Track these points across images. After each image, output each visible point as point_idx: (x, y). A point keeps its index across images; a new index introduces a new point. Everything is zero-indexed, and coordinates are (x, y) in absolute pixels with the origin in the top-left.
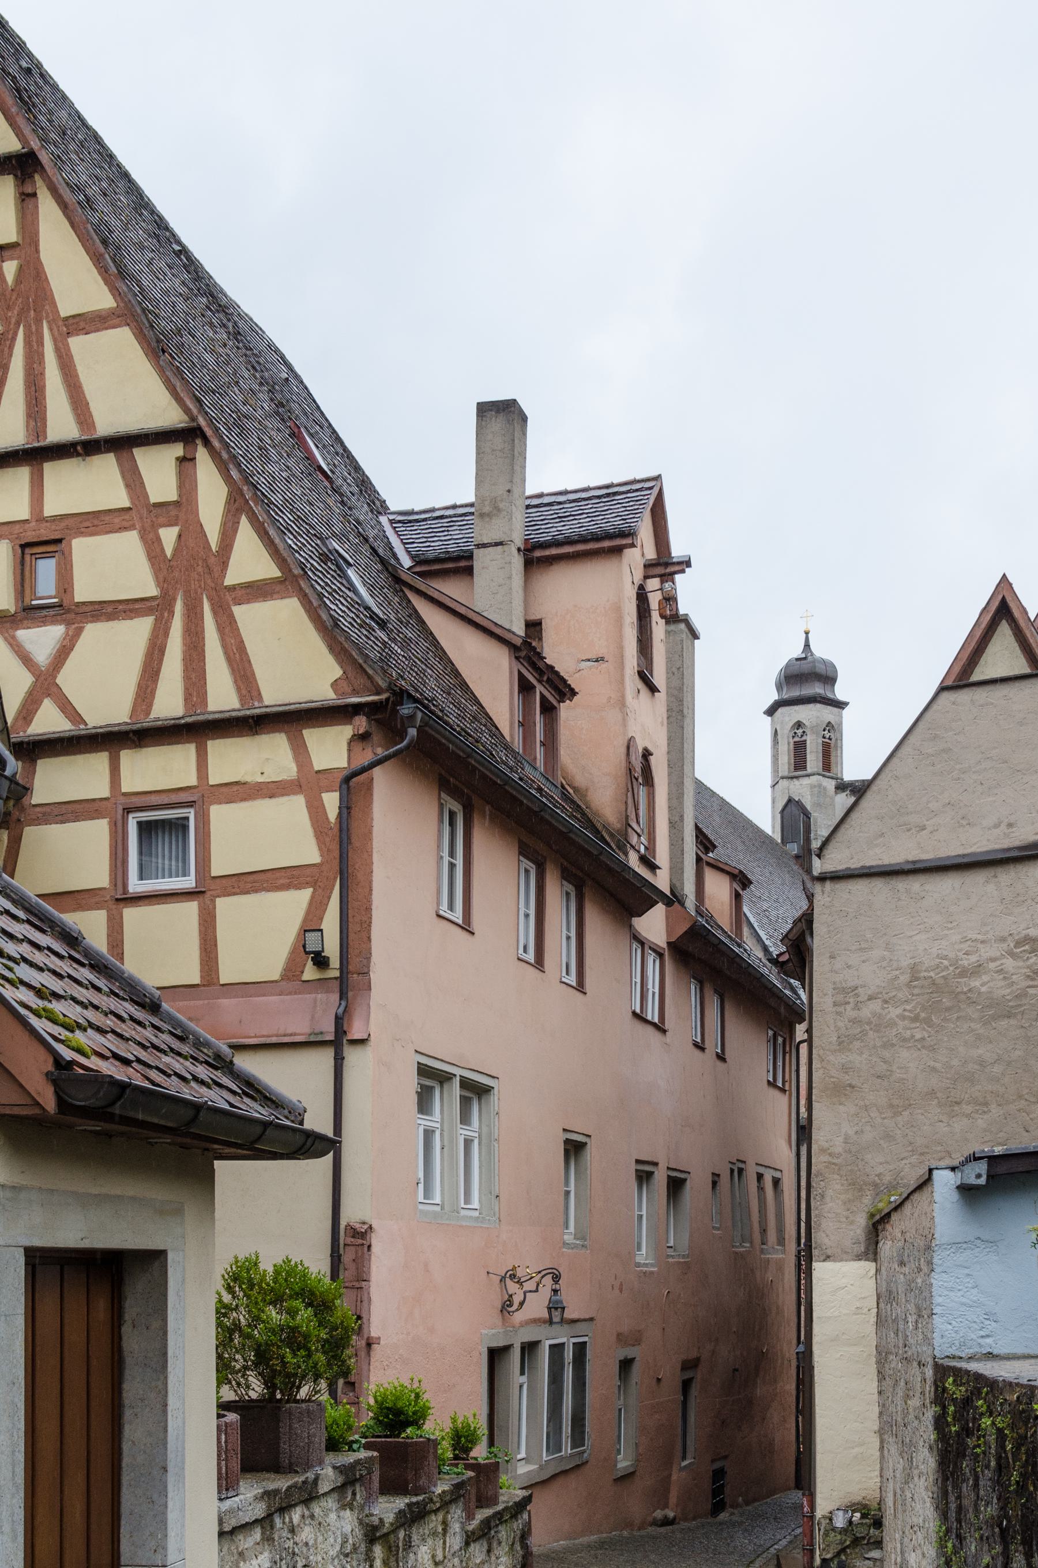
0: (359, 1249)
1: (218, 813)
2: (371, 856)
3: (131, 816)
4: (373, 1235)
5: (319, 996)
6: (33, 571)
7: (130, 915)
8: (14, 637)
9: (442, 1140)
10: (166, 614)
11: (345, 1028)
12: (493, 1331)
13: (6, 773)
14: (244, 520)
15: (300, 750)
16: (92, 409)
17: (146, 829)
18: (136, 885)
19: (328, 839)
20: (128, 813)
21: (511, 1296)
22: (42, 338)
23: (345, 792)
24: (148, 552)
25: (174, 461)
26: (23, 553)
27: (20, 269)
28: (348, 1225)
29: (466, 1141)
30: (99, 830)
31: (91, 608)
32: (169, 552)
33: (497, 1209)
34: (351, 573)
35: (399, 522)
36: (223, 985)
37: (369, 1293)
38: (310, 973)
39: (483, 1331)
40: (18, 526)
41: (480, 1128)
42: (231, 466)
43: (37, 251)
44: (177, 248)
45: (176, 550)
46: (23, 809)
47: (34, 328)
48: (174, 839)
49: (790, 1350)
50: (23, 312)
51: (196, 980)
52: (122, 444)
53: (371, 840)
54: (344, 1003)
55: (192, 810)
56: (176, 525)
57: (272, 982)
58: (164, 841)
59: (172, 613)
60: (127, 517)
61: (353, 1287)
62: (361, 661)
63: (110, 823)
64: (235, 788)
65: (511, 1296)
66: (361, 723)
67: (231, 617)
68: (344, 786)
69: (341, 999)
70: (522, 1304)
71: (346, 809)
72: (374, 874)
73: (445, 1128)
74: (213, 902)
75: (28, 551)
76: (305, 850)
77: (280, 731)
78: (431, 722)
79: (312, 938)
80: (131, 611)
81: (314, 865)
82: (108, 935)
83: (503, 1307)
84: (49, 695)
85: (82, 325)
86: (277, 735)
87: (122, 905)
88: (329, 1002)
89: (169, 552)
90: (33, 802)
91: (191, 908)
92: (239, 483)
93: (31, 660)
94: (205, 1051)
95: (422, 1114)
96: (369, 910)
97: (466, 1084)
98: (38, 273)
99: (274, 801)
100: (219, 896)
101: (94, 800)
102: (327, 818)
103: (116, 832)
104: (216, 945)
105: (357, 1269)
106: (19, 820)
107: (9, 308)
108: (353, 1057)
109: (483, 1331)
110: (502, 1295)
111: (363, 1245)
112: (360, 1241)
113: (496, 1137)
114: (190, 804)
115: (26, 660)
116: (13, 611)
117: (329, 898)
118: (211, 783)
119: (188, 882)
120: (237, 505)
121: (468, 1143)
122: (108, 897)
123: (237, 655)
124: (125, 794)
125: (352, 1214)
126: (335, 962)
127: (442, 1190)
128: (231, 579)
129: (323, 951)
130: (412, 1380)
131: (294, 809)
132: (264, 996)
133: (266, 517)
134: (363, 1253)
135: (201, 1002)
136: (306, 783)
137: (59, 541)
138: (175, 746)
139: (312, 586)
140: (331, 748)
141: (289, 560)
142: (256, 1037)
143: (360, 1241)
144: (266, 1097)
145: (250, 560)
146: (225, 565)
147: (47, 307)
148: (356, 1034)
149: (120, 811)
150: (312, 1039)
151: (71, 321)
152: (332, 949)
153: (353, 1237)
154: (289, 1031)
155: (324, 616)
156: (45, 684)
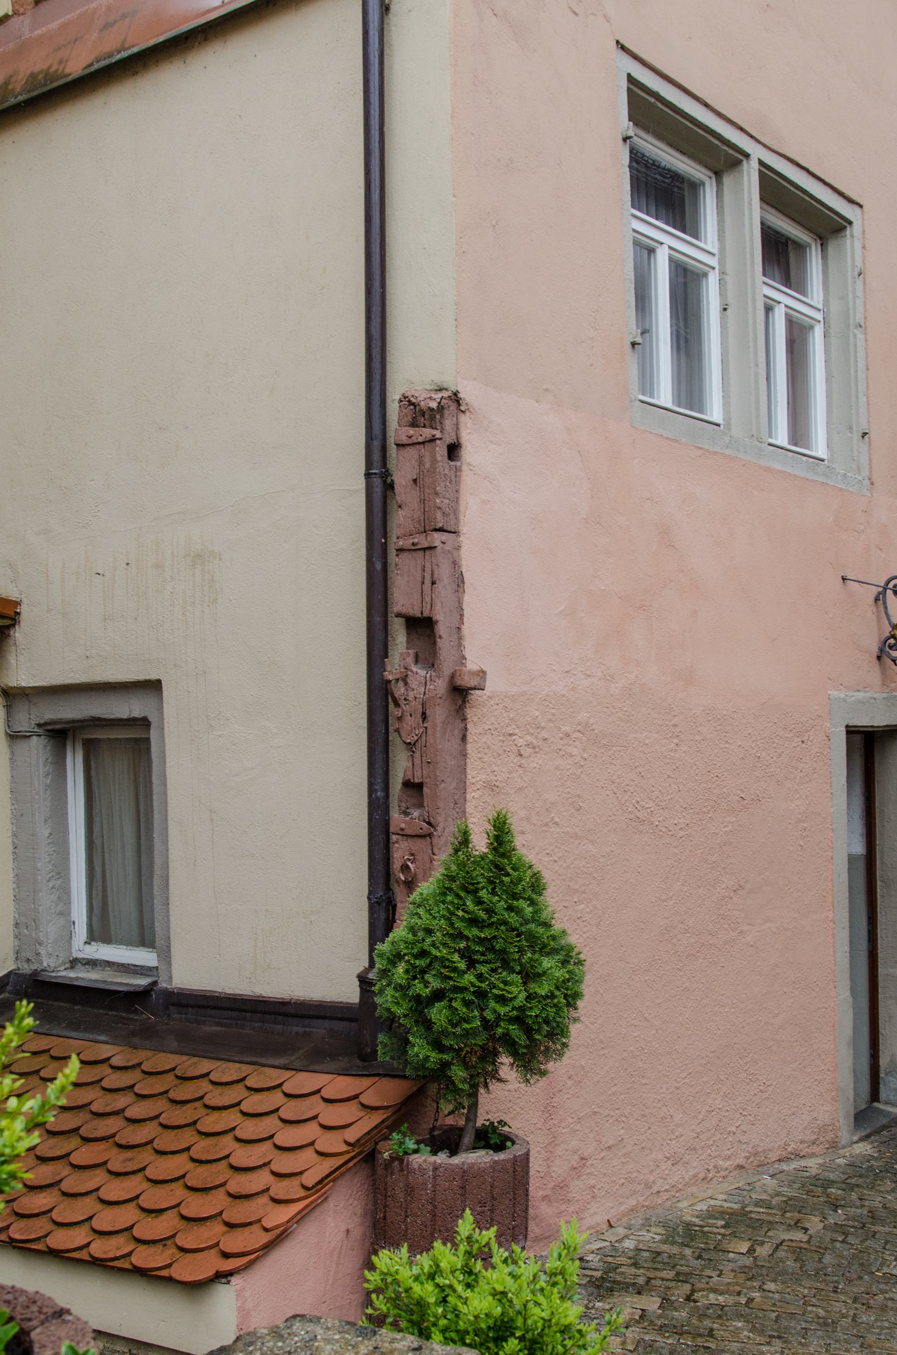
0: (425, 451)
12: (860, 695)
33: (864, 459)
37: (455, 564)
39: (834, 693)
41: (826, 302)
49: (262, 1060)
61: (414, 549)
73: (729, 268)
83: (881, 650)
95: (796, 445)
97: (776, 191)
105: (423, 501)
109: (834, 693)
112: (427, 433)
113: (859, 318)
121: (797, 334)
125: (414, 371)
127: (726, 397)
134: (434, 461)
143: (427, 433)
153: (414, 424)
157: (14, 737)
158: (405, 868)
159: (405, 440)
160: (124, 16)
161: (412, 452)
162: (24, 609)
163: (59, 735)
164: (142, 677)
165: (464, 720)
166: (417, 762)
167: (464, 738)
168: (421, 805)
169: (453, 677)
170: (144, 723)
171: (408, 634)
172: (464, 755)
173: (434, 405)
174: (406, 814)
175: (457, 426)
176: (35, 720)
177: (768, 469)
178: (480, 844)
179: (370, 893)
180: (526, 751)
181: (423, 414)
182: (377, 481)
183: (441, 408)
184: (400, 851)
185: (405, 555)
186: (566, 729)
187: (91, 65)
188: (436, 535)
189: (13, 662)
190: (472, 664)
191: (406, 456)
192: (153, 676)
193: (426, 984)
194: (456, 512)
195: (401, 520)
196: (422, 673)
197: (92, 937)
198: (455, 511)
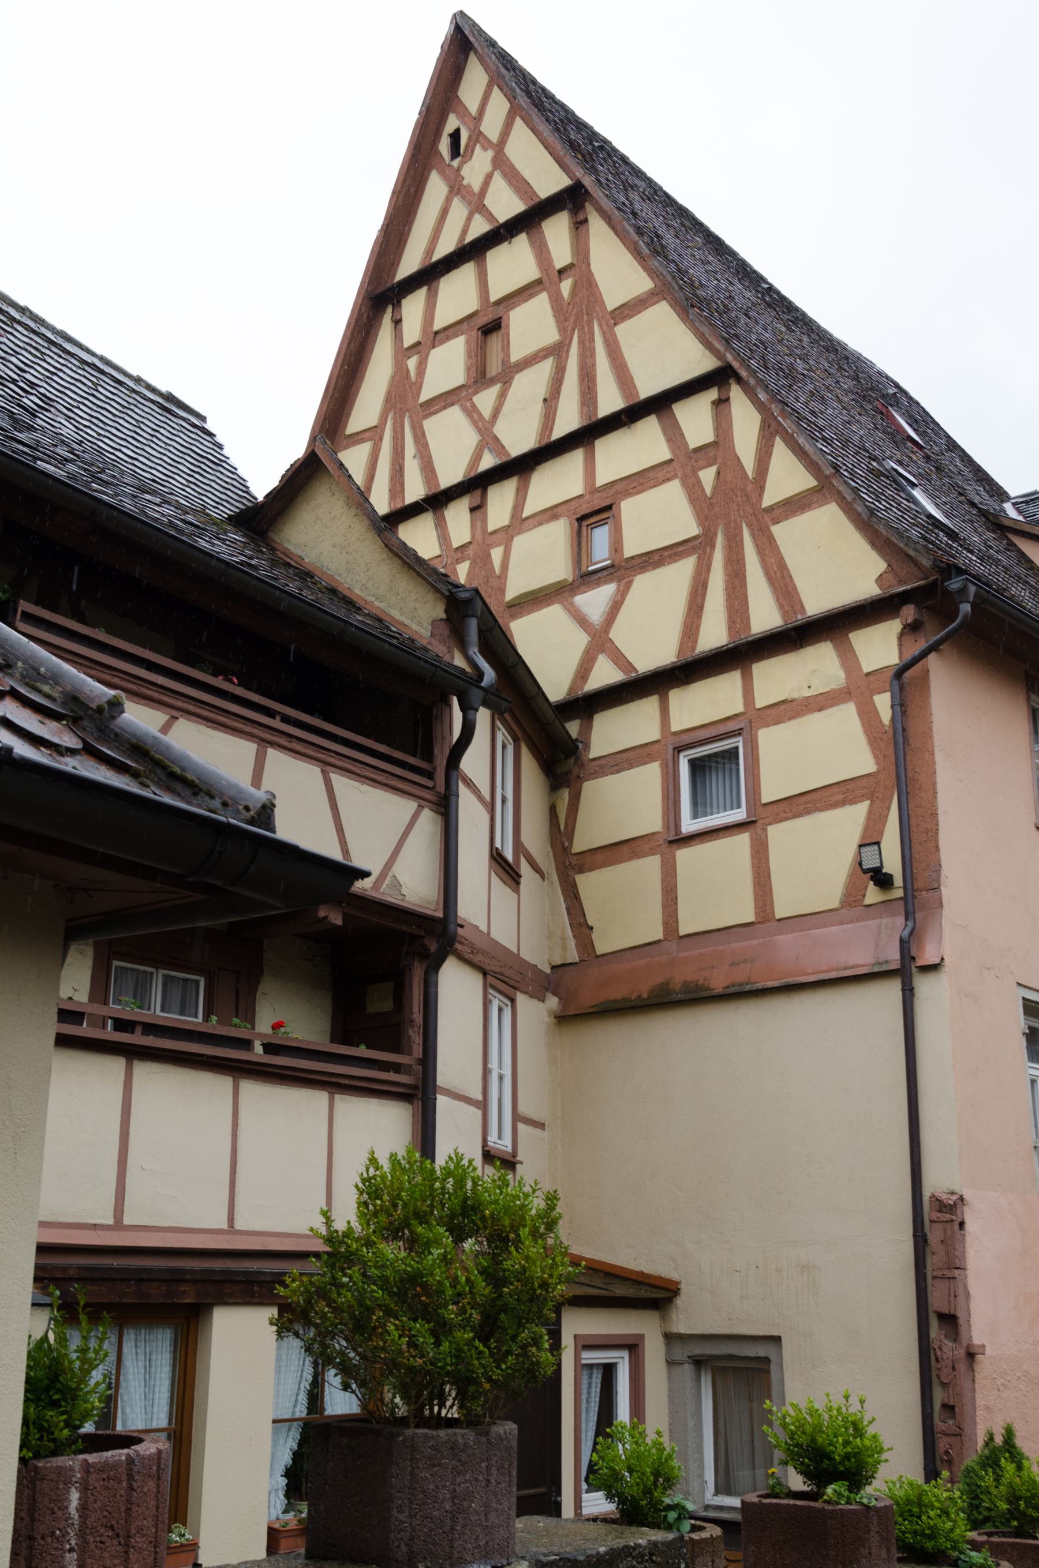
0: (948, 1226)
1: (766, 737)
2: (933, 754)
3: (682, 755)
4: (965, 1208)
5: (884, 921)
6: (589, 541)
7: (684, 856)
8: (572, 604)
10: (708, 550)
11: (913, 953)
13: (482, 684)
14: (778, 441)
15: (848, 657)
16: (637, 382)
17: (698, 767)
18: (689, 825)
19: (883, 745)
20: (679, 752)
22: (593, 335)
23: (897, 689)
24: (689, 496)
25: (709, 406)
26: (580, 526)
27: (575, 286)
28: (933, 1196)
30: (651, 774)
31: (639, 560)
32: (708, 490)
34: (917, 493)
35: (1022, 502)
36: (779, 920)
37: (965, 1286)
38: (873, 895)
40: (574, 503)
42: (759, 390)
43: (589, 265)
44: (766, 286)
45: (715, 488)
46: (582, 766)
47: (586, 329)
48: (727, 777)
50: (578, 318)
51: (751, 918)
52: (661, 404)
53: (931, 737)
54: (910, 924)
55: (740, 739)
56: (714, 464)
57: (831, 910)
58: (724, 778)
59: (713, 547)
60: (671, 468)
61: (943, 1277)
62: (901, 545)
63: (661, 765)
64: (783, 707)
66: (909, 612)
67: (771, 539)
68: (896, 682)
69: (907, 919)
71: (901, 706)
72: (938, 774)
74: (765, 830)
75: (585, 523)
76: (861, 761)
77: (825, 640)
78: (991, 598)
79: (869, 853)
80: (676, 554)
81: (869, 775)
82: (663, 881)
84: (603, 651)
85: (626, 312)
86: (823, 644)
87: (675, 846)
88: (896, 925)
89: (708, 490)
90: (591, 757)
91: (743, 839)
92: (767, 403)
93: (587, 621)
94: (46, 688)
96: (934, 815)
98: (590, 283)
99: (823, 713)
100: (770, 824)
101: (646, 745)
102: (881, 722)
103: (667, 773)
104: (769, 877)
105: (947, 1252)
106: (579, 777)
107: (566, 320)
108: (925, 987)
111: (952, 1221)
112: (948, 1217)
114: (737, 733)
115: (582, 621)
116: (570, 580)
117: (889, 808)
118: (758, 706)
119: (739, 815)
120: (769, 431)
122: (662, 841)
123: (778, 574)
124: (675, 734)
126: (898, 881)
128: (767, 501)
129: (882, 866)
130: (847, 1397)
131: (846, 717)
132: (824, 927)
133: (794, 427)
134: (953, 1232)
135: (756, 942)
136: (856, 689)
137: (609, 508)
138: (720, 676)
139: (845, 482)
140: (879, 646)
141: (820, 463)
142: (814, 973)
143: (948, 1217)
144: (172, 775)
145: (787, 476)
146: (762, 489)
147: (597, 308)
148: (929, 957)
149: (671, 751)
150: (876, 969)
151: (617, 313)
152: (893, 865)
153: (940, 1211)
154: (851, 964)
155: (860, 508)
156: (600, 641)
157: (670, 1363)
158: (947, 1453)
159: (935, 1219)
160: (745, 961)
161: (939, 1226)
163: (699, 1363)
164: (767, 1334)
165: (973, 1371)
167: (973, 1381)
170: (767, 1360)
171: (939, 1322)
172: (974, 1390)
173: (951, 1202)
174: (945, 1422)
175: (962, 1212)
176: (687, 1353)
178: (999, 1440)
181: (945, 1206)
183: (955, 1204)
184: (942, 1443)
185: (937, 1280)
186: (1018, 1374)
188: (956, 1271)
189: (675, 1318)
190: (976, 1341)
191: (935, 1230)
192: (776, 1334)
193: (980, 1513)
194: (964, 1258)
196: (950, 1344)
197: (717, 1492)
198: (963, 1258)
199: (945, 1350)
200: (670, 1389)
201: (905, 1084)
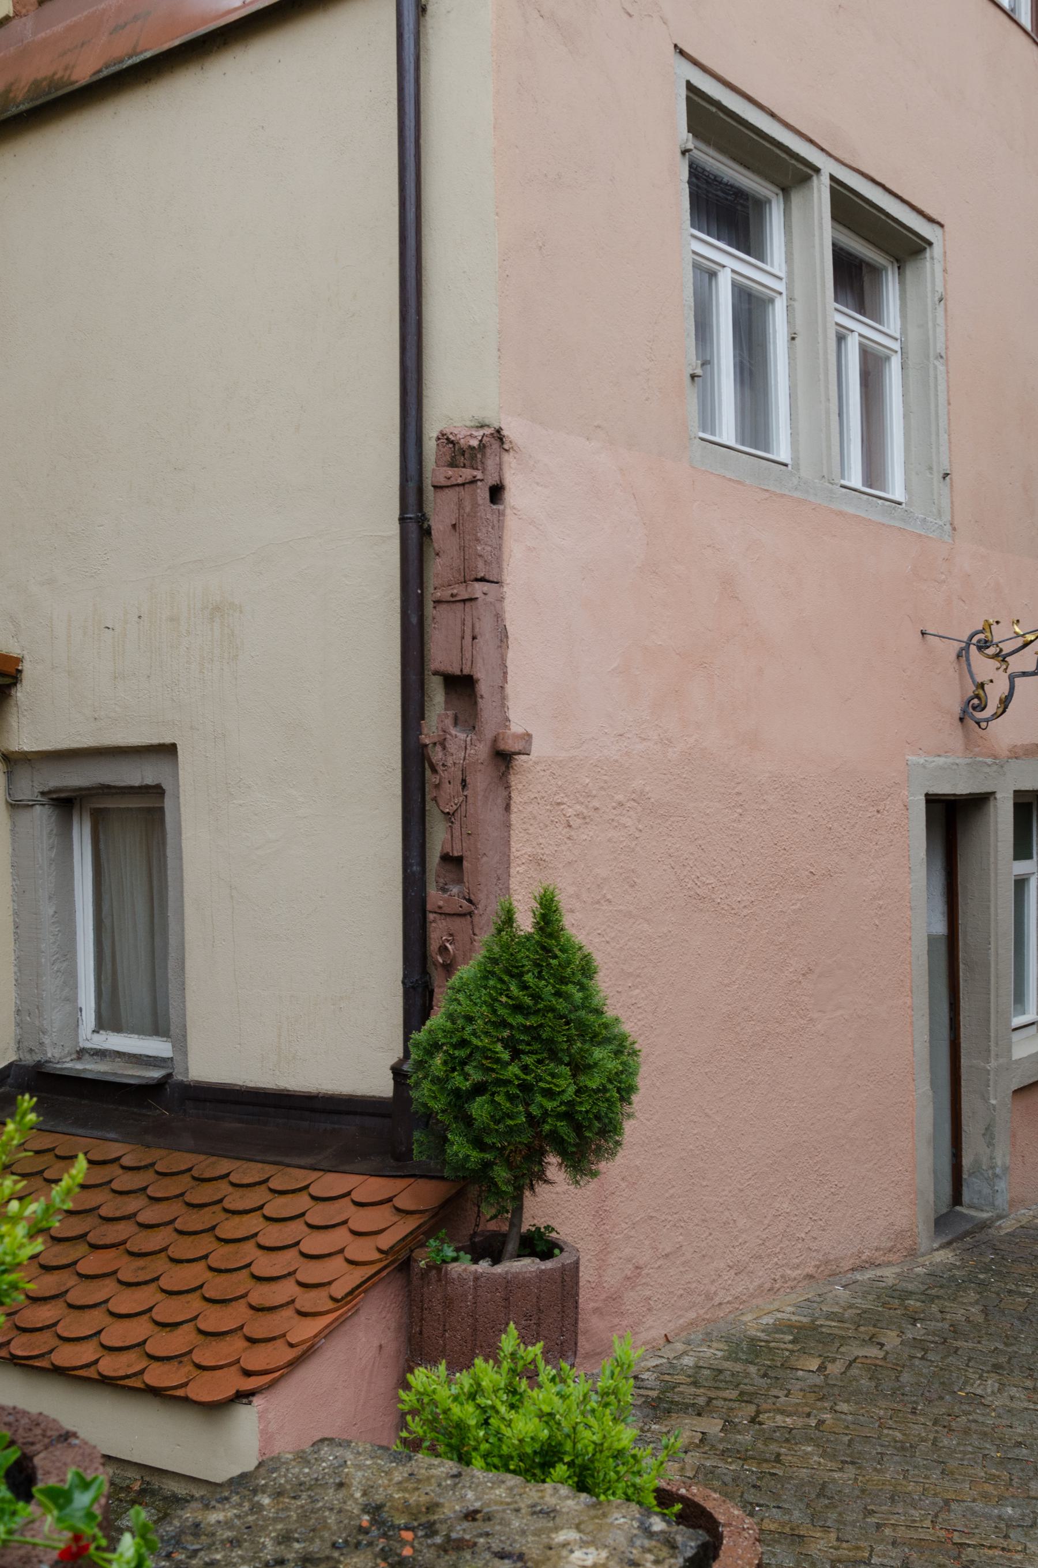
0: (465, 493)
9: (790, 322)
12: (941, 761)
21: (982, 686)
29: (866, 354)
33: (945, 503)
37: (499, 617)
38: (976, 701)
41: (904, 331)
61: (453, 601)
65: (982, 686)
70: (1005, 702)
73: (797, 294)
95: (870, 487)
105: (463, 548)
110: (962, 687)
112: (467, 473)
113: (940, 347)
121: (872, 367)
125: (454, 405)
134: (475, 505)
143: (467, 473)
153: (453, 464)
157: (15, 806)
158: (443, 950)
159: (443, 482)
161: (451, 494)
162: (26, 667)
164: (155, 741)
165: (508, 787)
166: (457, 833)
167: (507, 808)
168: (460, 881)
169: (495, 740)
170: (157, 791)
171: (447, 693)
172: (508, 826)
173: (475, 443)
174: (444, 890)
175: (500, 466)
177: (841, 513)
178: (525, 923)
179: (405, 976)
180: (576, 822)
181: (463, 453)
182: (413, 527)
183: (482, 447)
184: (438, 931)
186: (620, 797)
187: (100, 71)
188: (477, 585)
189: (15, 724)
191: (443, 501)
192: (167, 740)
193: (466, 1076)
194: (499, 560)
195: (439, 570)
199: (452, 747)
200: (15, 853)
201: (396, 209)
